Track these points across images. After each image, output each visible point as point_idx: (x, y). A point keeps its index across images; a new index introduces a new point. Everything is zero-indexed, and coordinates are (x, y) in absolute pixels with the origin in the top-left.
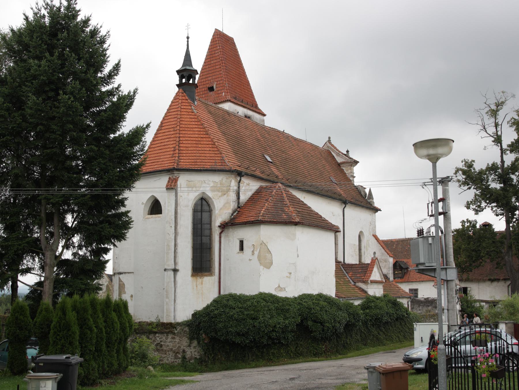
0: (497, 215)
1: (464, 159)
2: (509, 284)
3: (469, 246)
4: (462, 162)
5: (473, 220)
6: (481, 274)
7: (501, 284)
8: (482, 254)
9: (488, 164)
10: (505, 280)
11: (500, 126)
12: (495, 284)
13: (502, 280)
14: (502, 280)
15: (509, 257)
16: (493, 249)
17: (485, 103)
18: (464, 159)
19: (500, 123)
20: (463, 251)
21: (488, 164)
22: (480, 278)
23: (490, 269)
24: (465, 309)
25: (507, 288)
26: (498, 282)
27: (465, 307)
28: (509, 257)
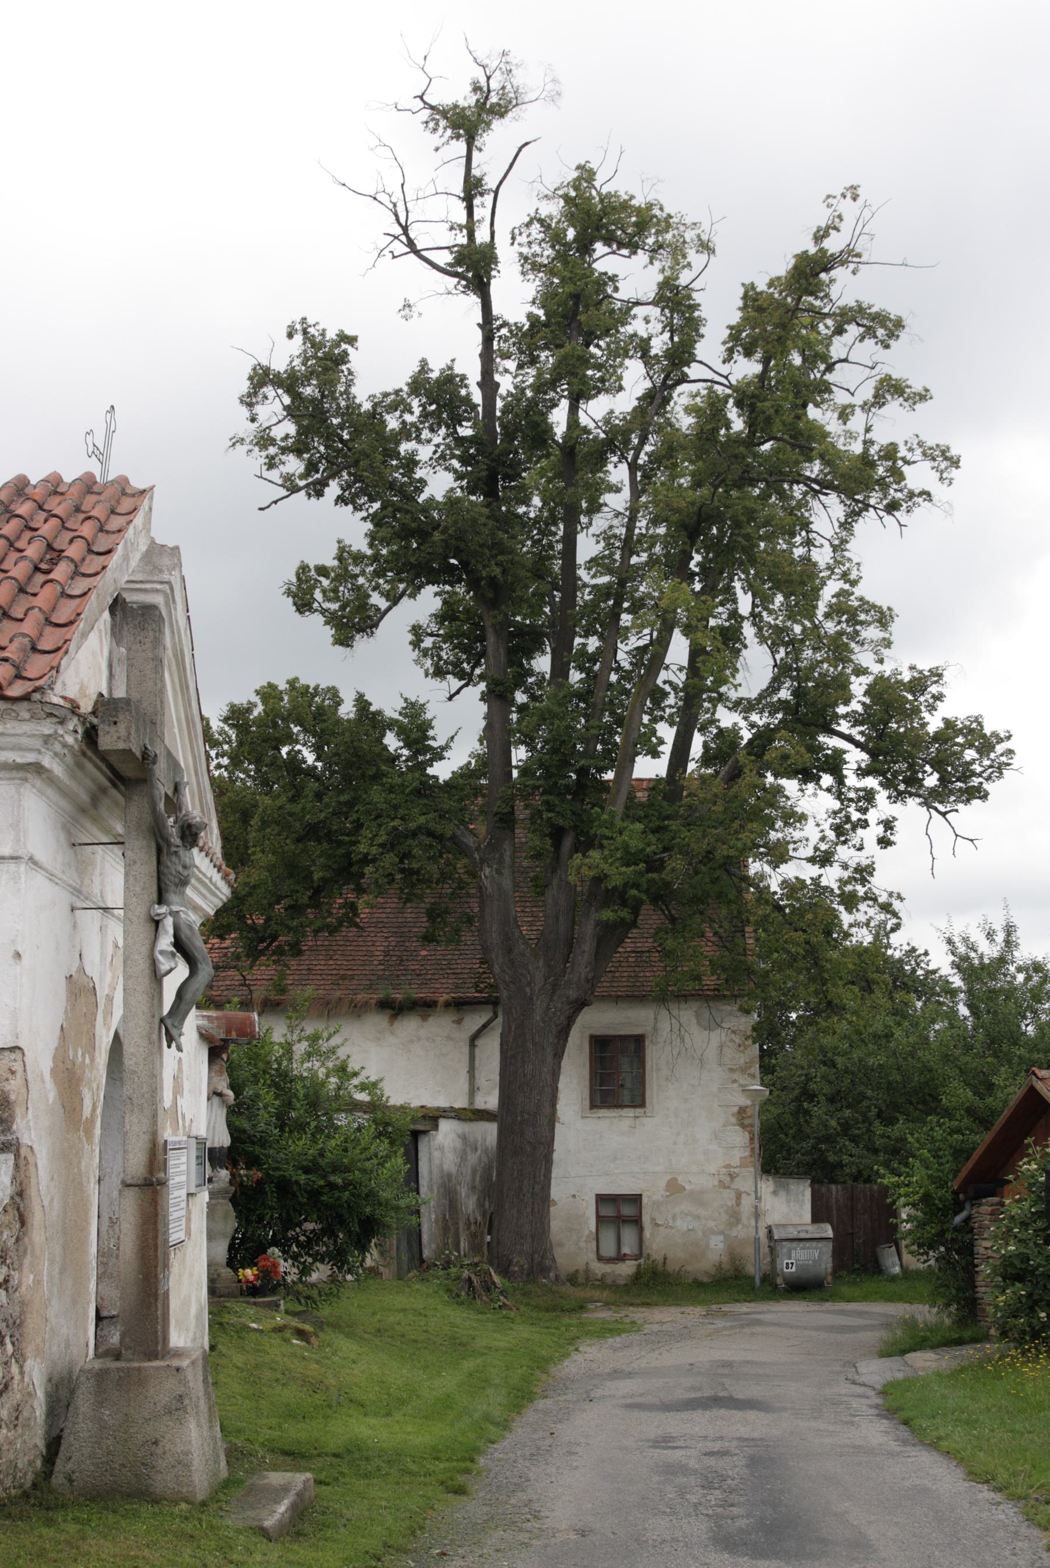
0: (439, 673)
1: (304, 320)
2: (475, 1028)
3: (296, 808)
4: (290, 336)
5: (323, 686)
6: (343, 977)
7: (440, 1025)
8: (363, 848)
9: (424, 363)
10: (460, 1006)
11: (489, 199)
12: (410, 1026)
13: (448, 1005)
14: (448, 1005)
15: (499, 872)
16: (422, 820)
17: (421, 97)
18: (304, 320)
19: (491, 183)
20: (265, 823)
21: (424, 363)
22: (338, 993)
23: (387, 953)
24: (263, 1143)
25: (466, 1050)
26: (424, 1018)
27: (264, 1121)
28: (499, 872)
